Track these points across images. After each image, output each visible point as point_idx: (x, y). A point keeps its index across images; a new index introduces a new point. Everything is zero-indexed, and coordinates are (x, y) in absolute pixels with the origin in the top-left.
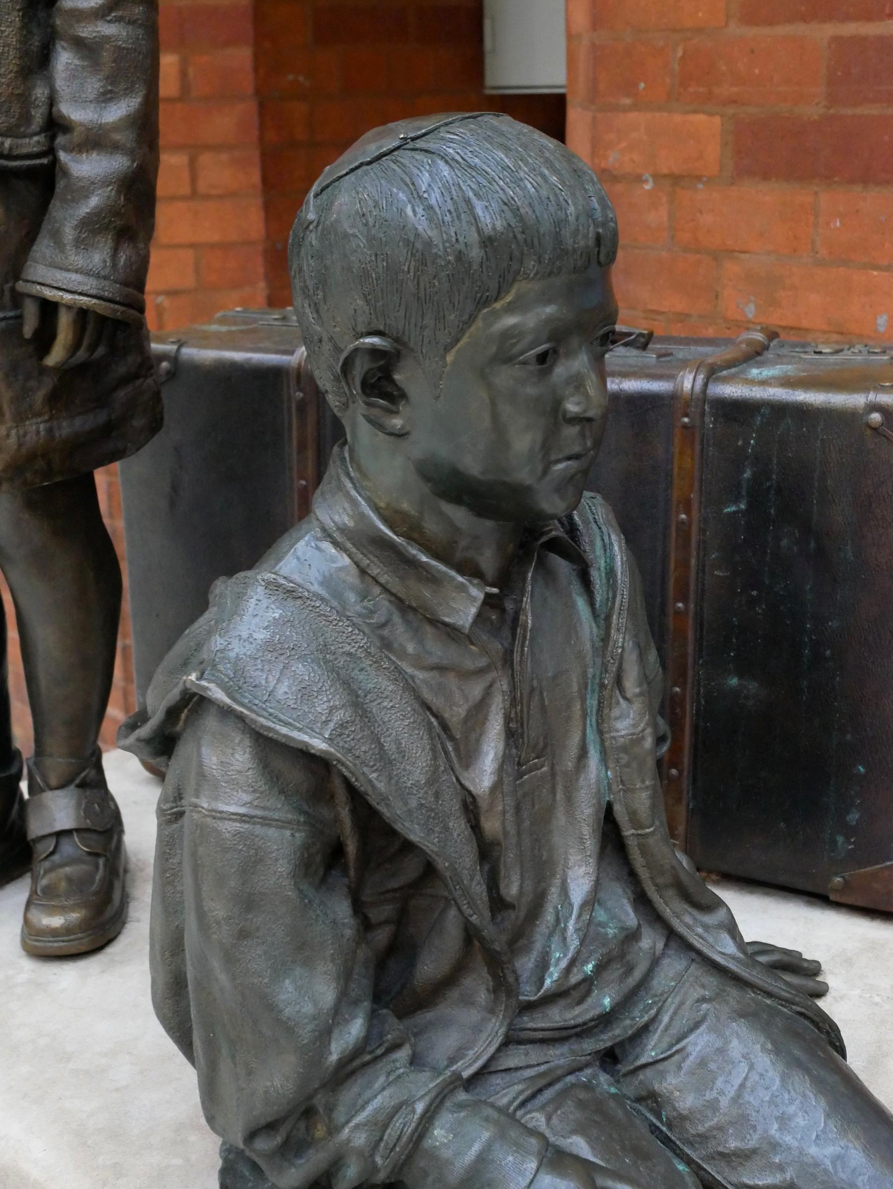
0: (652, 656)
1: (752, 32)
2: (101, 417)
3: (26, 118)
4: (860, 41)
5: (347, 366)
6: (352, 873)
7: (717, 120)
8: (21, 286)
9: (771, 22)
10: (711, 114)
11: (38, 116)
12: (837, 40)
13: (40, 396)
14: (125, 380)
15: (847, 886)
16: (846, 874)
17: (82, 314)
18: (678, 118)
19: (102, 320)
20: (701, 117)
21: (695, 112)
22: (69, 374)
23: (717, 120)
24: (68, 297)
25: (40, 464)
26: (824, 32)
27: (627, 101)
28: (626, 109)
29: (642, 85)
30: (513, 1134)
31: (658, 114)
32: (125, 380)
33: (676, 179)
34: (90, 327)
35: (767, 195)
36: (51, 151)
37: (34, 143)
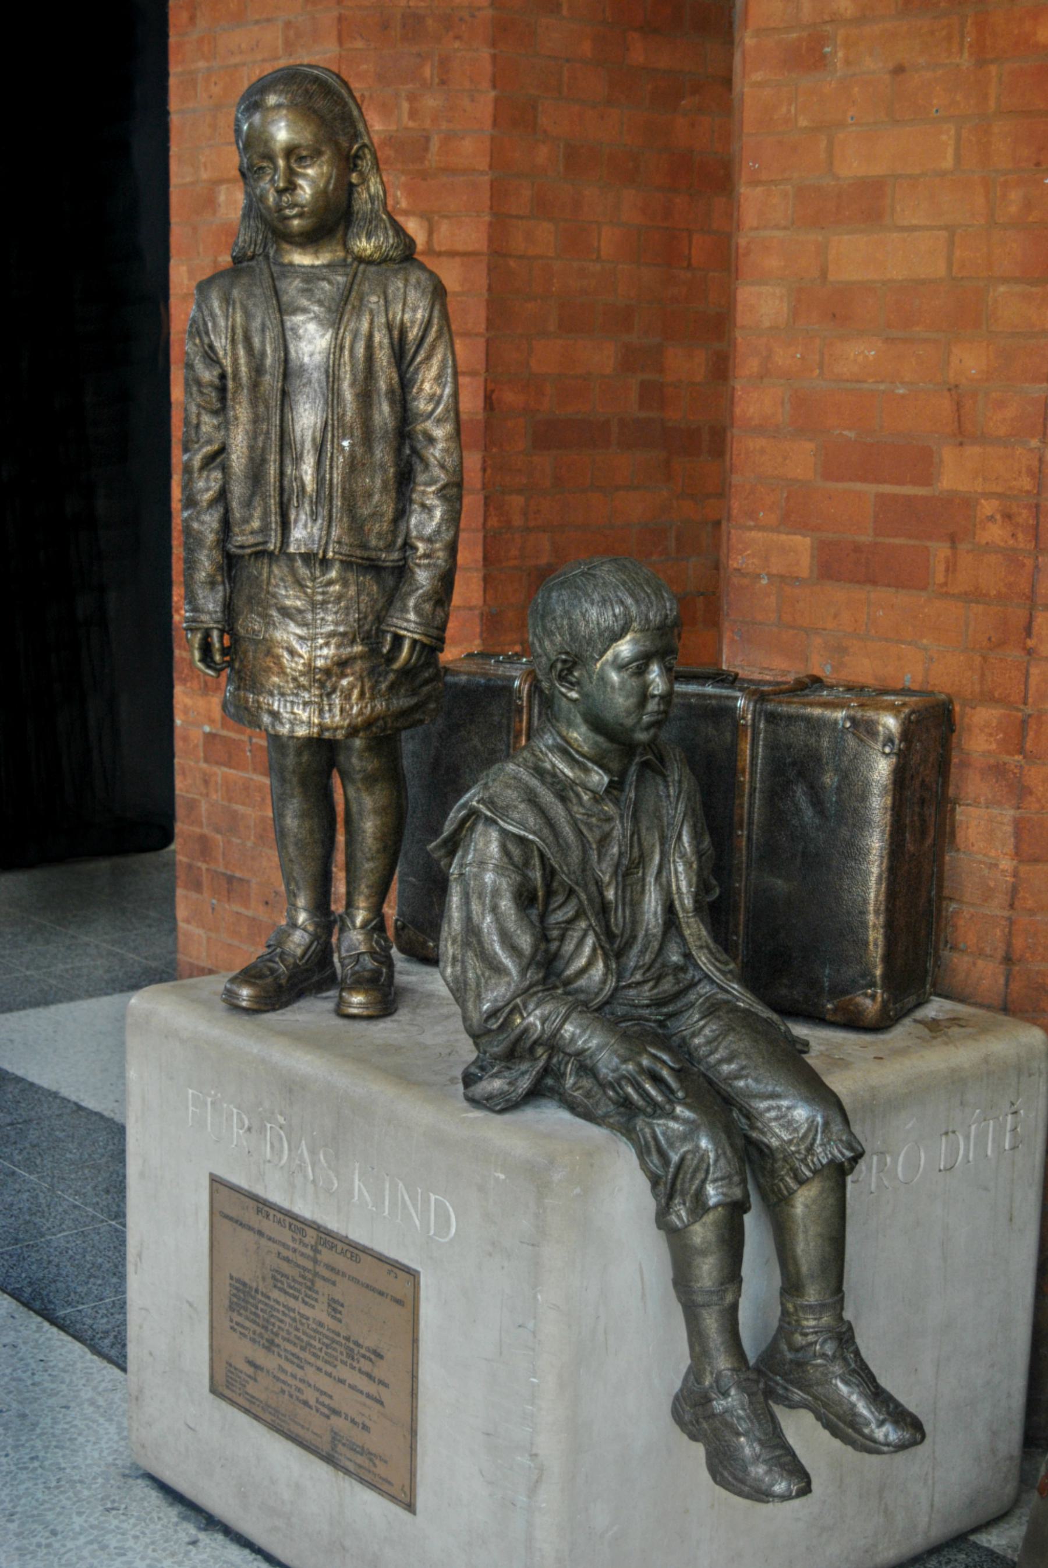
0: (707, 842)
2: (413, 701)
3: (394, 542)
4: (895, 497)
5: (552, 666)
6: (540, 907)
7: (808, 540)
8: (384, 627)
9: (840, 479)
10: (805, 536)
11: (400, 541)
12: (879, 496)
15: (835, 1010)
16: (835, 1002)
17: (414, 642)
19: (424, 646)
20: (799, 538)
21: (795, 534)
22: (407, 673)
24: (409, 634)
25: (381, 723)
26: (871, 489)
27: (752, 523)
28: (751, 529)
29: (761, 514)
31: (770, 534)
32: (426, 682)
33: (782, 577)
34: (418, 648)
35: (839, 593)
36: (405, 559)
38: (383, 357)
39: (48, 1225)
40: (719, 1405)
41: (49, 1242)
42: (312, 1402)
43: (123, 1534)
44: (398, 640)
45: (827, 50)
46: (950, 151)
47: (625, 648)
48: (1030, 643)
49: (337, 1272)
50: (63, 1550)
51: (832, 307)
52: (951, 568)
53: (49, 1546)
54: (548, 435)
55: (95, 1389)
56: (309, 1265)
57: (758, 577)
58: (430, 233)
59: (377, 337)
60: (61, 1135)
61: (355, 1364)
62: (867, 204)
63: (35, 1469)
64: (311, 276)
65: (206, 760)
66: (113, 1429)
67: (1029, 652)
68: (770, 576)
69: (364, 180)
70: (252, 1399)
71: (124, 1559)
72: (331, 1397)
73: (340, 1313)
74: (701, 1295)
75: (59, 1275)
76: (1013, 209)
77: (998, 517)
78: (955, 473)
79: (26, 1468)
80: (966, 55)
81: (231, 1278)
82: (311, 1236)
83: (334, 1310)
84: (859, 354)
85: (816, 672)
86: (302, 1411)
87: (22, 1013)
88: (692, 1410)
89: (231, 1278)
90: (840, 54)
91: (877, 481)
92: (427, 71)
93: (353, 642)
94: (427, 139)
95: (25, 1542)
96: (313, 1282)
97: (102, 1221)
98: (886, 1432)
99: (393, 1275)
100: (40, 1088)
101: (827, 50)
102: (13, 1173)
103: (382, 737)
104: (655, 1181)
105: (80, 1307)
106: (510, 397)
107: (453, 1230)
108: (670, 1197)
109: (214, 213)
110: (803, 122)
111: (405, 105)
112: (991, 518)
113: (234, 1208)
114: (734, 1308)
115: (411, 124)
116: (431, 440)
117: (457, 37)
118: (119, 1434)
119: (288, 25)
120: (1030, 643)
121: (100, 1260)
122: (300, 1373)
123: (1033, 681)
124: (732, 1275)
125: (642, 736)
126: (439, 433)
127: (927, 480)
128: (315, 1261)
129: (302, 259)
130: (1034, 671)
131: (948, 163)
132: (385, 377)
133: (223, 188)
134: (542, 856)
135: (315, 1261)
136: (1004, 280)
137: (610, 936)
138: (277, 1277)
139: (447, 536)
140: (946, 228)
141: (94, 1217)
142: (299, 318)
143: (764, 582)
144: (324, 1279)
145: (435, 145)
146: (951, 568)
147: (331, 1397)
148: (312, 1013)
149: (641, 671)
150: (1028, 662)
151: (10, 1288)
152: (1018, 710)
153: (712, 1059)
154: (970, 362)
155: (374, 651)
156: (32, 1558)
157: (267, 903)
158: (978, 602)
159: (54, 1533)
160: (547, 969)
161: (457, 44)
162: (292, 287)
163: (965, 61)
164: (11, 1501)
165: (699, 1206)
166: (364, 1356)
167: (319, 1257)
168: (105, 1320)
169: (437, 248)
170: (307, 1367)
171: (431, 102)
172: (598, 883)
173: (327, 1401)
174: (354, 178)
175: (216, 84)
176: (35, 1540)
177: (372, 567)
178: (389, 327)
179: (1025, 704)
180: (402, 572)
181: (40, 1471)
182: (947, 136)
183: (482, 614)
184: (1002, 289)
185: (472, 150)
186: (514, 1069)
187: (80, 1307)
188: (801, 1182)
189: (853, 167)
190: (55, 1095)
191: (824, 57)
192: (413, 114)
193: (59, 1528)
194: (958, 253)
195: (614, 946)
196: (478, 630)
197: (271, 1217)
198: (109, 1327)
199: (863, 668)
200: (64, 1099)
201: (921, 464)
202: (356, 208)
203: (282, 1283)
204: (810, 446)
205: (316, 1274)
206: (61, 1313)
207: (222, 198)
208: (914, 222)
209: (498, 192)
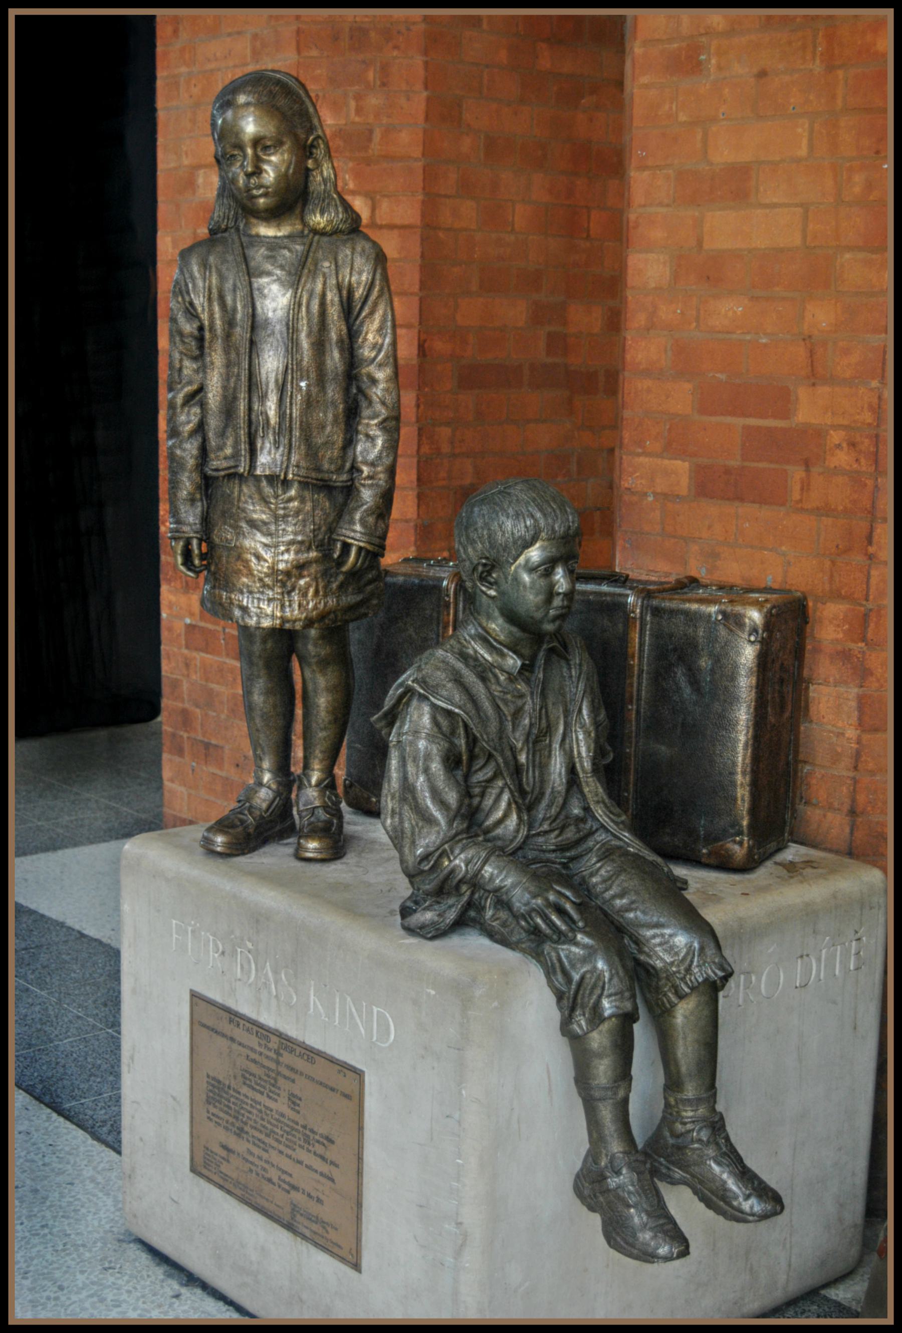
0: (602, 715)
1: (705, 418)
2: (359, 598)
3: (343, 466)
4: (759, 429)
5: (475, 569)
6: (465, 769)
7: (687, 464)
8: (335, 536)
10: (684, 461)
12: (746, 428)
13: (334, 586)
14: (370, 582)
17: (360, 549)
18: (666, 462)
20: (679, 462)
21: (676, 459)
22: (354, 574)
23: (687, 464)
24: (356, 542)
25: (332, 616)
27: (640, 450)
28: (639, 455)
30: (515, 776)
31: (655, 460)
32: (370, 582)
33: (665, 495)
34: (363, 554)
35: (712, 509)
36: (352, 480)
37: (344, 477)
38: (334, 312)
39: (56, 1032)
40: (613, 1182)
41: (57, 1046)
42: (275, 1180)
43: (118, 1289)
44: (346, 547)
45: (703, 57)
46: (805, 142)
47: (535, 554)
48: (871, 550)
49: (296, 1072)
50: (68, 1303)
51: (707, 271)
52: (805, 487)
53: (57, 1299)
54: (471, 377)
55: (95, 1168)
56: (273, 1066)
57: (645, 494)
58: (373, 209)
59: (329, 296)
60: (67, 958)
61: (310, 1148)
62: (736, 185)
63: (45, 1235)
64: (274, 245)
65: (187, 647)
66: (109, 1202)
67: (870, 557)
68: (655, 494)
69: (318, 165)
70: (225, 1177)
71: (119, 1309)
72: (291, 1175)
73: (298, 1105)
74: (598, 1090)
75: (65, 1074)
76: (857, 190)
77: (844, 445)
78: (808, 410)
79: (38, 1234)
80: (818, 62)
81: (208, 1076)
82: (274, 1042)
83: (294, 1103)
84: (729, 310)
85: (693, 573)
86: (267, 1188)
87: (34, 857)
88: (591, 1186)
89: (208, 1076)
90: (713, 61)
91: (744, 415)
92: (371, 75)
93: (309, 549)
94: (371, 132)
95: (37, 1295)
96: (275, 1080)
97: (101, 1029)
98: (751, 1205)
99: (342, 1074)
100: (49, 919)
101: (703, 57)
102: (27, 990)
103: (333, 627)
104: (560, 996)
105: (83, 1101)
106: (439, 346)
107: (392, 1037)
108: (573, 1009)
109: (194, 193)
110: (682, 117)
111: (353, 104)
112: (839, 446)
113: (211, 1019)
114: (625, 1101)
115: (357, 119)
116: (374, 381)
117: (396, 47)
118: (115, 1206)
119: (255, 37)
120: (871, 550)
121: (99, 1062)
122: (265, 1156)
123: (873, 581)
124: (624, 1074)
125: (549, 627)
126: (380, 375)
127: (785, 414)
128: (278, 1063)
129: (266, 231)
130: (874, 573)
131: (803, 152)
132: (336, 329)
133: (201, 172)
134: (466, 726)
135: (278, 1063)
136: (849, 248)
137: (523, 792)
138: (246, 1076)
139: (387, 461)
140: (801, 205)
141: (94, 1026)
142: (264, 280)
143: (651, 499)
144: (285, 1077)
145: (377, 135)
146: (805, 487)
147: (291, 1175)
148: (275, 856)
149: (548, 573)
150: (870, 566)
151: (24, 1084)
152: (861, 605)
153: (607, 895)
154: (821, 316)
155: (326, 556)
156: (43, 1309)
157: (238, 765)
158: (827, 516)
159: (61, 1288)
160: (470, 821)
161: (395, 53)
162: (258, 255)
163: (817, 67)
164: (25, 1261)
165: (596, 1017)
166: (318, 1142)
167: (281, 1059)
168: (103, 1112)
169: (379, 222)
170: (270, 1150)
171: (374, 101)
172: (513, 749)
173: (288, 1179)
174: (310, 164)
175: (195, 85)
176: (45, 1294)
177: (324, 487)
178: (339, 287)
179: (867, 600)
180: (350, 490)
181: (49, 1237)
182: (802, 129)
183: (416, 526)
184: (847, 256)
185: (408, 140)
186: (444, 904)
187: (83, 1101)
188: (681, 997)
189: (724, 154)
190: (62, 925)
191: (699, 63)
192: (359, 111)
193: (65, 1284)
194: (811, 226)
195: (526, 802)
196: (413, 539)
197: (241, 1026)
198: (107, 1117)
199: (733, 570)
200: (69, 928)
201: (781, 401)
202: (311, 189)
203: (251, 1081)
204: (688, 386)
205: (279, 1073)
206: (67, 1106)
207: (200, 180)
208: (775, 200)
209: (430, 175)
